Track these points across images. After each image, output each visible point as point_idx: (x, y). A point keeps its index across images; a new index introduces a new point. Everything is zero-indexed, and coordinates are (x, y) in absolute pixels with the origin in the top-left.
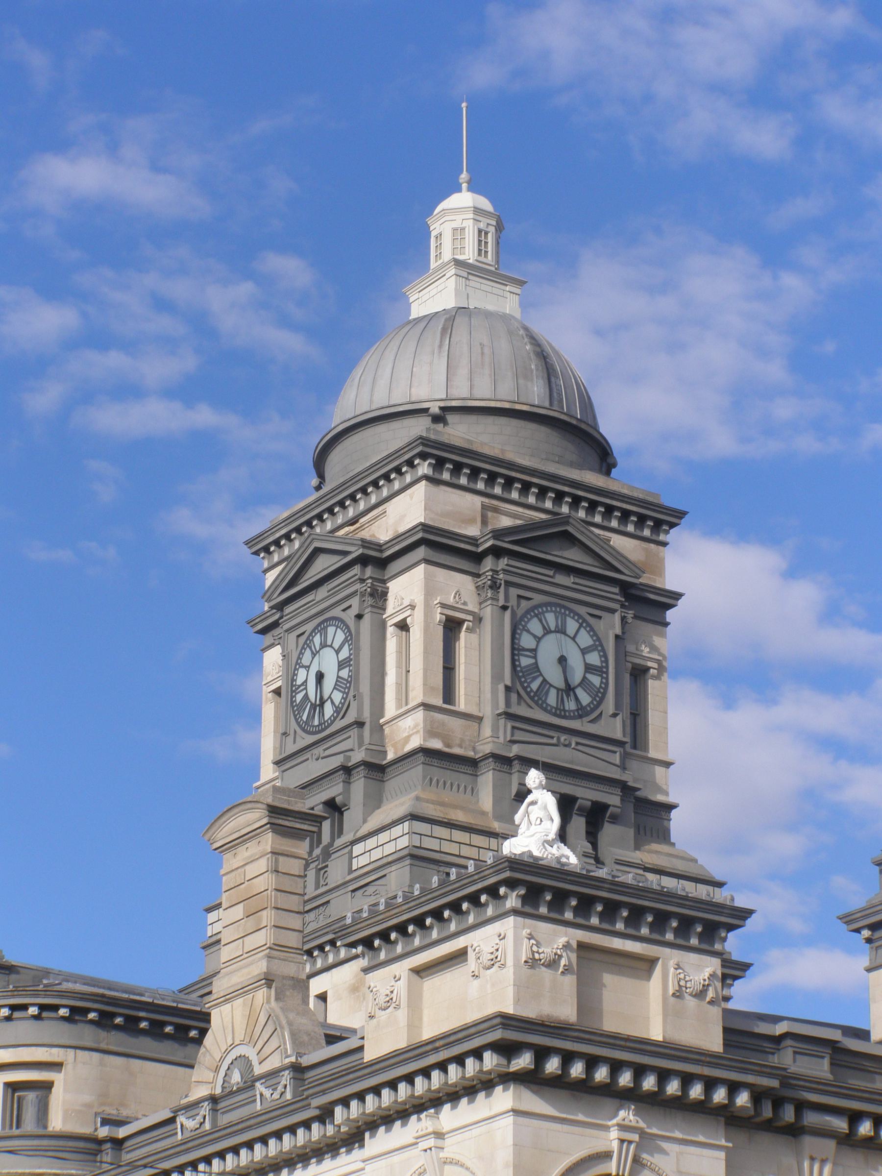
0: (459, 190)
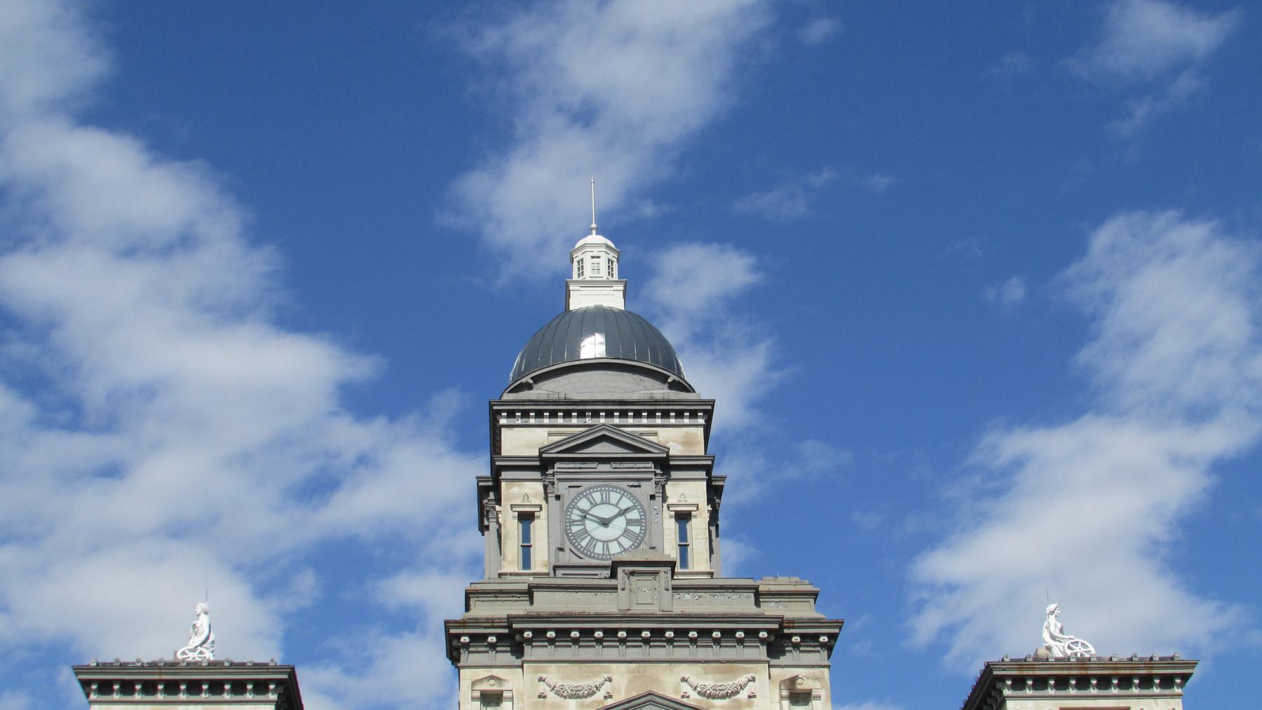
0: (589, 233)
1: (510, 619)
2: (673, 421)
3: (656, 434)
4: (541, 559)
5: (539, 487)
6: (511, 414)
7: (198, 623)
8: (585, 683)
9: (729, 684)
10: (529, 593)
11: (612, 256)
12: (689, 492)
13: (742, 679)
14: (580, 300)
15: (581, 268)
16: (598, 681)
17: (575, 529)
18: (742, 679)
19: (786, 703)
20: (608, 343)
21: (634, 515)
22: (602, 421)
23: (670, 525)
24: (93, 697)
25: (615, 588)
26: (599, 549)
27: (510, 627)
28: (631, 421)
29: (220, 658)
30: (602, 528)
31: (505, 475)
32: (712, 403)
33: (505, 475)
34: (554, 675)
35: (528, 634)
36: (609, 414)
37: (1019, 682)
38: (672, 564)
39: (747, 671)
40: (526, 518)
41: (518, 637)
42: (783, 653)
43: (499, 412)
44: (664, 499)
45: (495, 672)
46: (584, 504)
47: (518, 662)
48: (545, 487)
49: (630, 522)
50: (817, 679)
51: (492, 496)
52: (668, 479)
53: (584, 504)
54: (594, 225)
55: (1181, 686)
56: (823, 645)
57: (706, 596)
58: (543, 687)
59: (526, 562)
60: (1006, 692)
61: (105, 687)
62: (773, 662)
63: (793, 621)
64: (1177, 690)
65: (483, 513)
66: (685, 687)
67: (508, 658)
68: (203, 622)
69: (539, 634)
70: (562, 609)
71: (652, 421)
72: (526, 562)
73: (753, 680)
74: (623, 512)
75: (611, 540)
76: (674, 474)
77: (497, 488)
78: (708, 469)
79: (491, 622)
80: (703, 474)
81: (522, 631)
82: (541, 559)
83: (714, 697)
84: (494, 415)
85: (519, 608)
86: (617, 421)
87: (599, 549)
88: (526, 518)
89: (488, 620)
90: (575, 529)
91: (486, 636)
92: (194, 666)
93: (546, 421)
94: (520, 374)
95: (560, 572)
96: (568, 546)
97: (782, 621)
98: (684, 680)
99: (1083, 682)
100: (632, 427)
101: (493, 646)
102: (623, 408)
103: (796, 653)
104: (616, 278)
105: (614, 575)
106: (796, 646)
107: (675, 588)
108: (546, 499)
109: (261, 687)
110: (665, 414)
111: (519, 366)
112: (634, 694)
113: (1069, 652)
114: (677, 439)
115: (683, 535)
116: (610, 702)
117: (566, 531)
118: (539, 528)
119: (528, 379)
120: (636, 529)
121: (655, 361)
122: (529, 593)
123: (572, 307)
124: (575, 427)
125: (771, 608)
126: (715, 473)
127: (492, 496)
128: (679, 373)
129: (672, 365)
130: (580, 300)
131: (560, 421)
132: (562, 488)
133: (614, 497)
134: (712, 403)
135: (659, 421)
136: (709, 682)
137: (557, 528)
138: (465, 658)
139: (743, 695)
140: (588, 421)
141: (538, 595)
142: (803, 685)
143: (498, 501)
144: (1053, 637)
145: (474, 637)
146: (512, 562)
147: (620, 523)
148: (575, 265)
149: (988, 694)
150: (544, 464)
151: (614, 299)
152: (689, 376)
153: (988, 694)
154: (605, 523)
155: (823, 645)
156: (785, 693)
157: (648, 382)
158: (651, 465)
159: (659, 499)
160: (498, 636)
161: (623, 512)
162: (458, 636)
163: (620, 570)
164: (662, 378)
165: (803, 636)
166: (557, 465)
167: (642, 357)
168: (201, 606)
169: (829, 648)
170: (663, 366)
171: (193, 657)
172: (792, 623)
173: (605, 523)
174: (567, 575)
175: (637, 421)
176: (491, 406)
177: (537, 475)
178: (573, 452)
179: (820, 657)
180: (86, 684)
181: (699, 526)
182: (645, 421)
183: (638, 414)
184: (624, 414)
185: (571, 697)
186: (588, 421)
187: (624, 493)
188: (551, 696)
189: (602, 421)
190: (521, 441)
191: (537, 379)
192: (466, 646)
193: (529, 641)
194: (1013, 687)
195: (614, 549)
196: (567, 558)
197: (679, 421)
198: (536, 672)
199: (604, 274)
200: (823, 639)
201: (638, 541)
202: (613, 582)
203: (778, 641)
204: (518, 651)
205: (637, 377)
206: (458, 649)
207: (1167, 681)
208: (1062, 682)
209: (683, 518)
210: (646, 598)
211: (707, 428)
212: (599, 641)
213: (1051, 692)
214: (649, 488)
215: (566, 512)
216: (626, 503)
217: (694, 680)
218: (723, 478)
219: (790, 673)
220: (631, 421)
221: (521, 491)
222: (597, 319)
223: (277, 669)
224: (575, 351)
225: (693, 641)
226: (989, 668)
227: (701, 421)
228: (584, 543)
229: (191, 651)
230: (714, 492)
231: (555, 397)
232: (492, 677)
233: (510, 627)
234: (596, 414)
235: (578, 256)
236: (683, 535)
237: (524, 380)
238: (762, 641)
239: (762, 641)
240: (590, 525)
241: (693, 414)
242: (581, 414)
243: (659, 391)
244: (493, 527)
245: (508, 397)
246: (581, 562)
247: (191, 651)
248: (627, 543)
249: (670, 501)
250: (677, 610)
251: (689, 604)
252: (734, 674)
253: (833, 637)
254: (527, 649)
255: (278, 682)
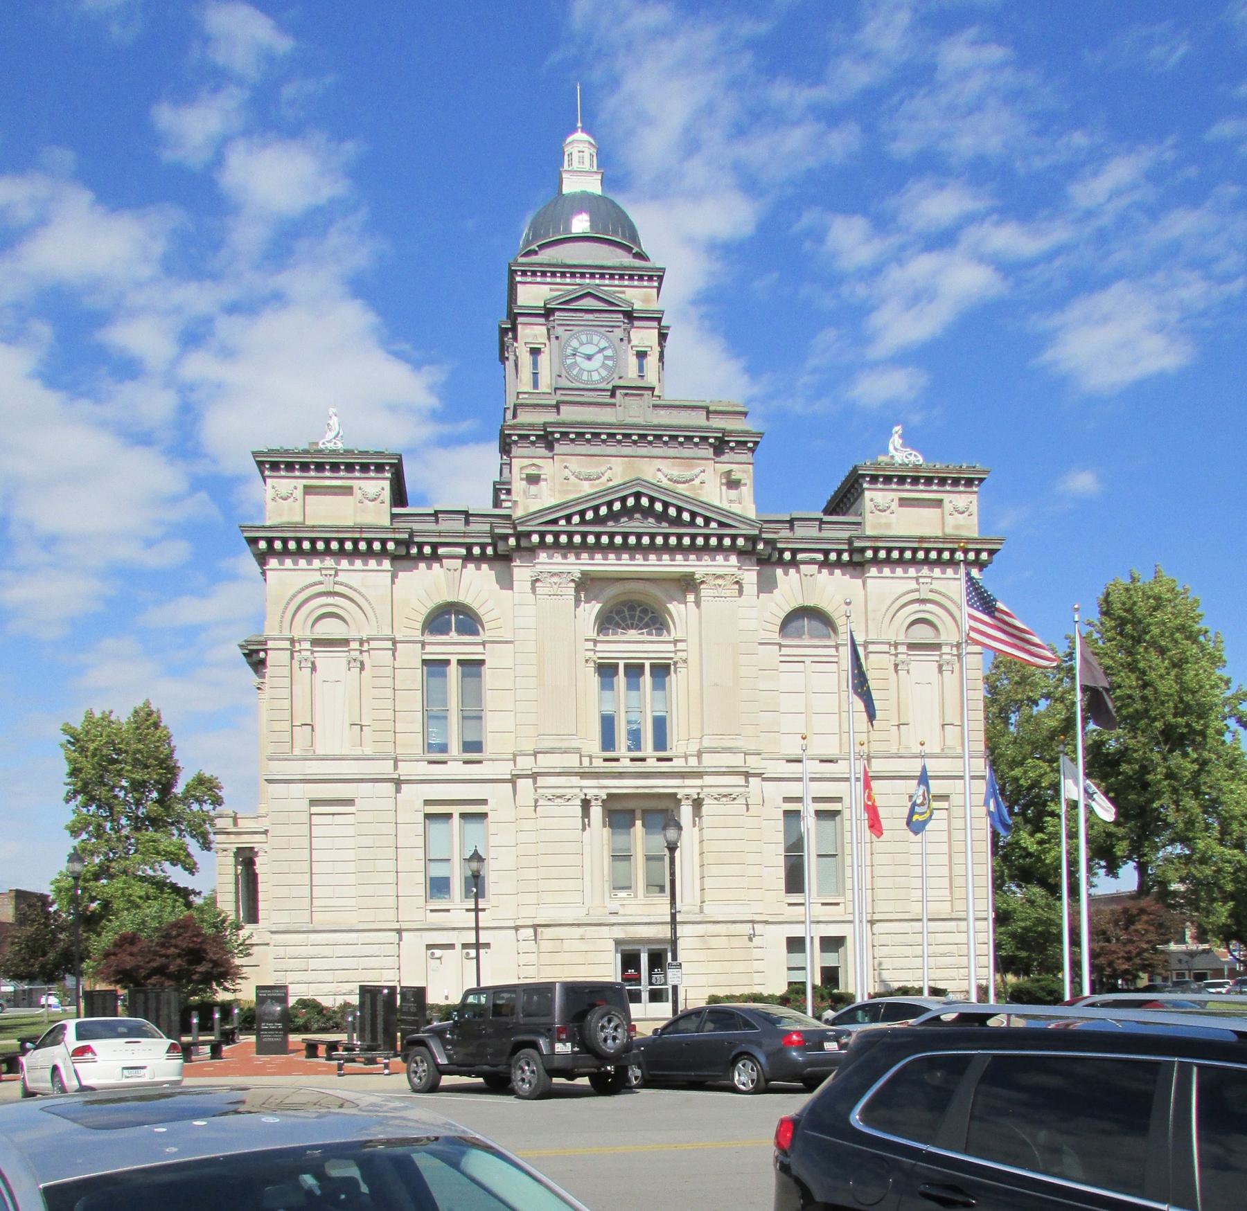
0: (574, 130)
1: (545, 425)
2: (636, 283)
3: (623, 292)
4: (545, 384)
5: (544, 329)
6: (524, 273)
7: (331, 422)
8: (594, 471)
9: (688, 474)
10: (557, 407)
11: (593, 151)
12: (645, 337)
13: (697, 471)
14: (571, 186)
15: (570, 160)
16: (603, 469)
17: (569, 361)
18: (697, 471)
19: (724, 488)
20: (591, 221)
21: (609, 353)
22: (587, 281)
23: (633, 361)
24: (267, 473)
25: (614, 405)
26: (585, 377)
27: (545, 430)
28: (607, 282)
29: (350, 447)
30: (587, 362)
31: (520, 320)
32: (663, 270)
33: (520, 320)
34: (575, 464)
35: (557, 436)
36: (592, 276)
37: (874, 479)
38: (652, 389)
39: (700, 465)
40: (535, 352)
41: (550, 438)
42: (723, 453)
43: (516, 271)
44: (629, 341)
45: (535, 461)
46: (575, 343)
47: (550, 454)
48: (548, 330)
49: (606, 358)
50: (744, 472)
51: (510, 335)
52: (633, 327)
53: (575, 343)
54: (579, 125)
55: (978, 486)
56: (750, 449)
57: (675, 412)
58: (567, 473)
59: (536, 385)
60: (865, 485)
61: (275, 466)
62: (718, 459)
63: (731, 432)
64: (975, 489)
65: (503, 348)
66: (660, 475)
67: (543, 451)
68: (334, 421)
69: (565, 435)
70: (579, 419)
71: (621, 283)
72: (536, 385)
73: (704, 471)
74: (601, 351)
75: (593, 371)
76: (636, 323)
77: (514, 329)
78: (659, 320)
79: (532, 426)
80: (655, 324)
81: (553, 433)
82: (545, 384)
83: (679, 482)
84: (512, 273)
85: (551, 417)
86: (597, 281)
87: (585, 377)
88: (535, 352)
89: (530, 425)
90: (569, 361)
91: (529, 436)
92: (334, 452)
93: (549, 280)
94: (528, 243)
95: (559, 392)
96: (564, 374)
97: (724, 431)
98: (659, 470)
99: (320, 467)
100: (608, 287)
101: (533, 443)
102: (602, 272)
103: (732, 454)
104: (595, 169)
105: (613, 395)
106: (732, 449)
107: (654, 406)
108: (549, 338)
109: (380, 468)
110: (631, 277)
111: (528, 235)
112: (627, 479)
113: (906, 461)
114: (637, 296)
115: (641, 368)
116: (611, 484)
117: (563, 363)
118: (544, 359)
119: (534, 247)
120: (610, 363)
121: (624, 237)
122: (557, 407)
123: (565, 191)
124: (569, 286)
125: (717, 423)
126: (663, 324)
127: (510, 335)
128: (639, 246)
129: (634, 237)
130: (571, 186)
131: (558, 280)
132: (559, 331)
133: (596, 339)
134: (663, 270)
135: (626, 283)
136: (675, 473)
137: (556, 360)
138: (515, 451)
139: (697, 482)
140: (578, 281)
141: (563, 408)
142: (735, 476)
143: (515, 339)
144: (896, 449)
145: (521, 437)
146: (525, 385)
147: (600, 357)
148: (566, 157)
149: (852, 486)
150: (548, 313)
151: (593, 186)
152: (646, 248)
153: (852, 486)
154: (589, 358)
155: (750, 449)
156: (724, 481)
157: (619, 252)
158: (621, 316)
159: (626, 342)
160: (537, 436)
161: (601, 351)
162: (510, 435)
163: (618, 392)
164: (629, 249)
165: (737, 442)
166: (557, 314)
167: (615, 233)
168: (332, 410)
169: (752, 450)
170: (628, 240)
171: (331, 446)
172: (730, 433)
173: (589, 358)
174: (565, 395)
175: (611, 282)
176: (510, 267)
177: (542, 320)
178: (568, 304)
179: (747, 457)
180: (260, 464)
181: (652, 361)
182: (617, 282)
183: (612, 277)
184: (602, 276)
185: (586, 479)
186: (578, 281)
187: (602, 335)
188: (572, 478)
189: (587, 281)
190: (531, 294)
191: (541, 247)
192: (515, 442)
193: (558, 440)
194: (870, 482)
195: (595, 377)
196: (564, 383)
197: (641, 284)
198: (563, 461)
199: (587, 166)
200: (750, 445)
201: (611, 370)
202: (613, 401)
203: (720, 446)
204: (550, 447)
205: (611, 248)
206: (509, 445)
207: (969, 482)
208: (305, 467)
209: (641, 355)
210: (633, 412)
211: (659, 289)
212: (604, 441)
213: (894, 486)
214: (619, 333)
215: (562, 349)
216: (603, 344)
217: (665, 470)
218: (668, 328)
219: (728, 467)
220: (607, 282)
221: (532, 333)
222: (584, 202)
223: (391, 456)
224: (568, 228)
225: (666, 443)
226: (855, 469)
227: (656, 284)
228: (575, 372)
229: (329, 442)
230: (663, 337)
231: (554, 261)
232: (534, 465)
233: (545, 430)
234: (583, 275)
235: (567, 150)
236: (641, 368)
237: (532, 247)
238: (711, 445)
239: (711, 445)
240: (579, 360)
241: (650, 278)
242: (573, 275)
243: (628, 260)
244: (512, 358)
245: (521, 260)
246: (572, 385)
247: (329, 442)
248: (604, 373)
249: (633, 343)
250: (656, 421)
251: (663, 418)
252: (691, 467)
253: (756, 443)
254: (556, 445)
255: (391, 465)
